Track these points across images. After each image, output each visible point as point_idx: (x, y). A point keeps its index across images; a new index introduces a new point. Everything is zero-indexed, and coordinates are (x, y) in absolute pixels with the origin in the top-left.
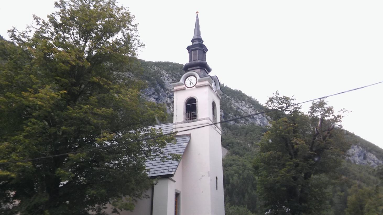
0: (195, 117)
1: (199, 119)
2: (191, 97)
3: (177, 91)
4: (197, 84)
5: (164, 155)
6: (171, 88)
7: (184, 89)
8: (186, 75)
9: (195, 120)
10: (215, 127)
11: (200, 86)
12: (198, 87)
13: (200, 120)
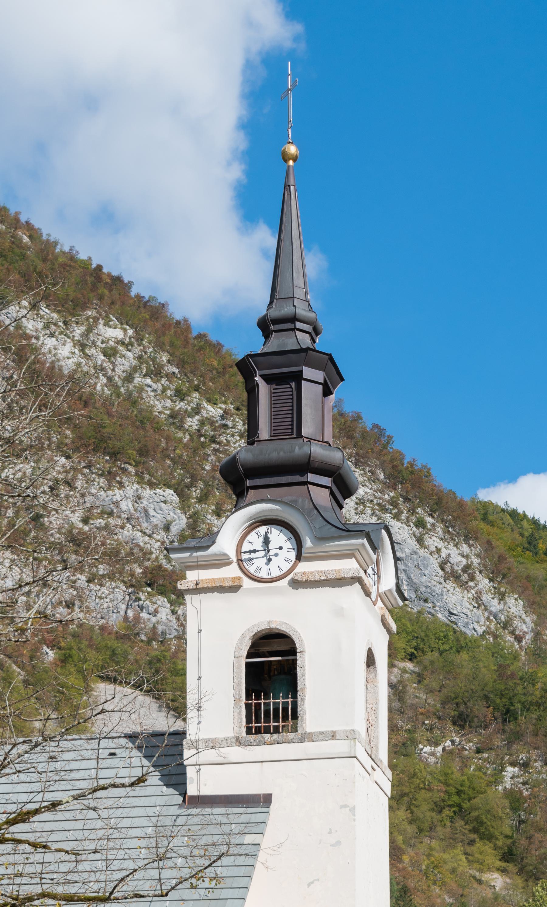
0: (290, 723)
1: (311, 734)
2: (272, 626)
3: (198, 590)
4: (297, 570)
5: (16, 888)
6: (73, 584)
7: (235, 588)
8: (263, 511)
9: (291, 735)
10: (372, 768)
11: (317, 578)
12: (296, 584)
13: (306, 738)
